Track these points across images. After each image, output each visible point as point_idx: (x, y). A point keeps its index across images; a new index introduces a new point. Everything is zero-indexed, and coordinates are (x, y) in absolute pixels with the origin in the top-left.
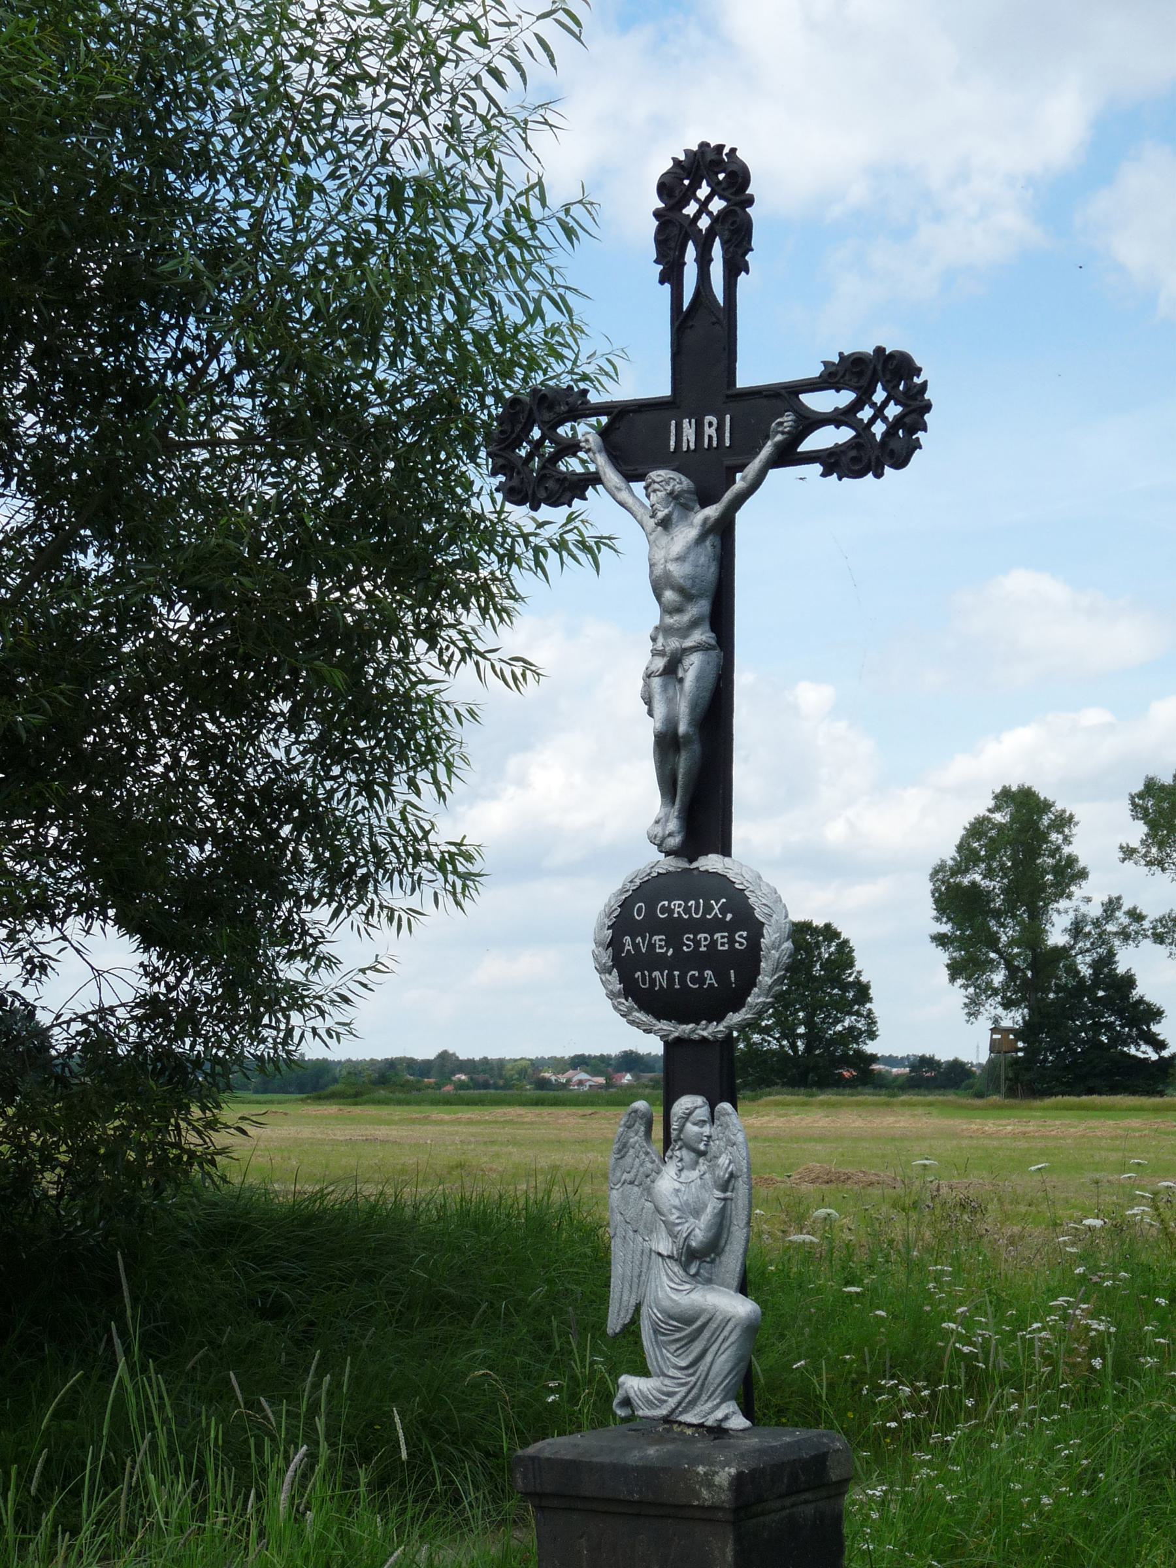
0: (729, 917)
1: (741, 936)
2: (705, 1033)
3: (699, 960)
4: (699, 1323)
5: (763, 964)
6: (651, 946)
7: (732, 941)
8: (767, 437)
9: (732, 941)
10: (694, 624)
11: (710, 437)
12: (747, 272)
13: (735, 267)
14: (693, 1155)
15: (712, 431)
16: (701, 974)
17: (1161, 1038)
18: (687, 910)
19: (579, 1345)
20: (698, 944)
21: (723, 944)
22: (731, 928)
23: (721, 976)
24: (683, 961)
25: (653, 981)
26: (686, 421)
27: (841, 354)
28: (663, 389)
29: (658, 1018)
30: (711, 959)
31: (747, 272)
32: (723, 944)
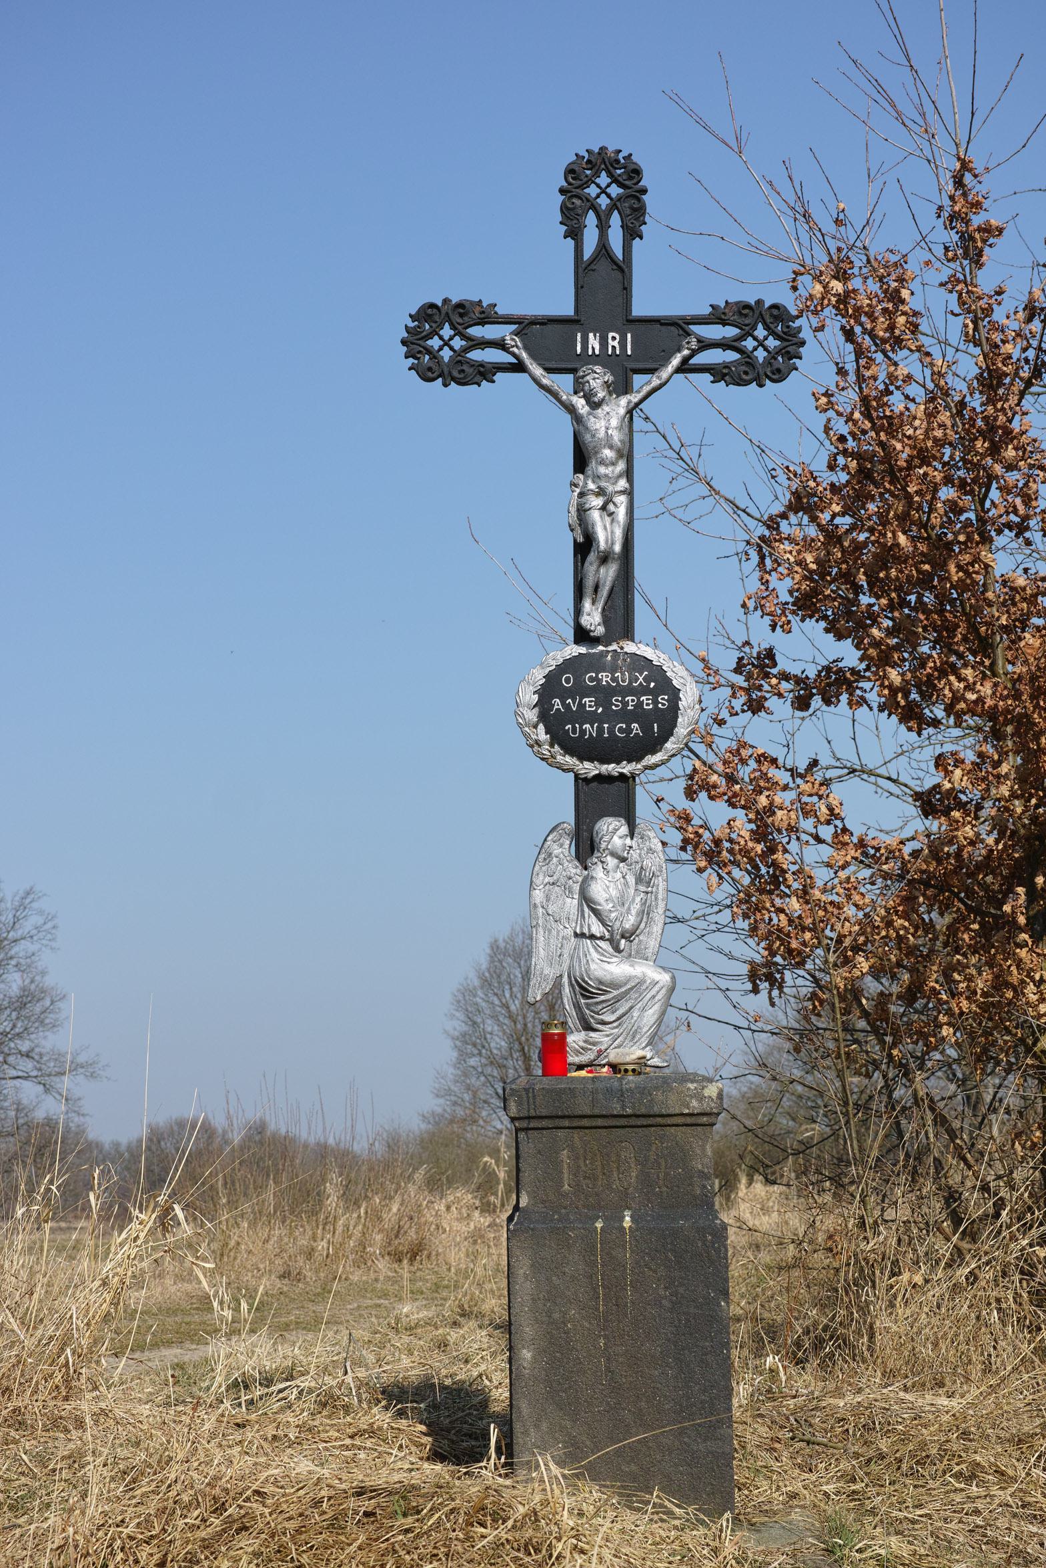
0: (652, 685)
1: (663, 700)
2: (624, 771)
3: (626, 716)
4: (629, 986)
5: (680, 720)
6: (582, 706)
7: (655, 702)
8: (679, 351)
9: (655, 702)
10: (620, 476)
11: (614, 347)
12: (641, 238)
13: (632, 233)
14: (616, 861)
15: (616, 343)
16: (628, 726)
17: (488, 951)
18: (614, 679)
19: (29, 1181)
20: (626, 704)
21: (648, 704)
22: (655, 693)
23: (647, 728)
24: (609, 716)
25: (583, 732)
26: (591, 335)
27: (726, 302)
28: (568, 310)
29: (581, 759)
30: (638, 714)
31: (641, 238)
32: (648, 704)
